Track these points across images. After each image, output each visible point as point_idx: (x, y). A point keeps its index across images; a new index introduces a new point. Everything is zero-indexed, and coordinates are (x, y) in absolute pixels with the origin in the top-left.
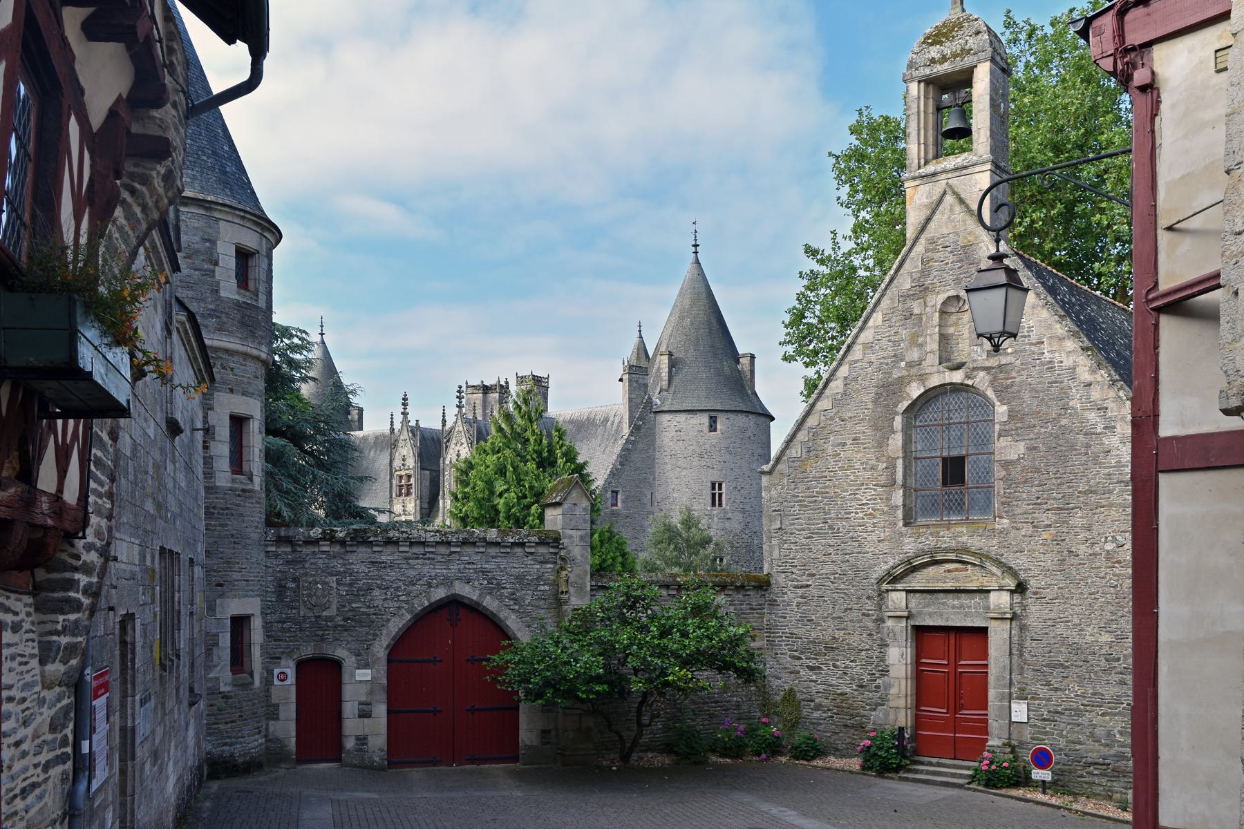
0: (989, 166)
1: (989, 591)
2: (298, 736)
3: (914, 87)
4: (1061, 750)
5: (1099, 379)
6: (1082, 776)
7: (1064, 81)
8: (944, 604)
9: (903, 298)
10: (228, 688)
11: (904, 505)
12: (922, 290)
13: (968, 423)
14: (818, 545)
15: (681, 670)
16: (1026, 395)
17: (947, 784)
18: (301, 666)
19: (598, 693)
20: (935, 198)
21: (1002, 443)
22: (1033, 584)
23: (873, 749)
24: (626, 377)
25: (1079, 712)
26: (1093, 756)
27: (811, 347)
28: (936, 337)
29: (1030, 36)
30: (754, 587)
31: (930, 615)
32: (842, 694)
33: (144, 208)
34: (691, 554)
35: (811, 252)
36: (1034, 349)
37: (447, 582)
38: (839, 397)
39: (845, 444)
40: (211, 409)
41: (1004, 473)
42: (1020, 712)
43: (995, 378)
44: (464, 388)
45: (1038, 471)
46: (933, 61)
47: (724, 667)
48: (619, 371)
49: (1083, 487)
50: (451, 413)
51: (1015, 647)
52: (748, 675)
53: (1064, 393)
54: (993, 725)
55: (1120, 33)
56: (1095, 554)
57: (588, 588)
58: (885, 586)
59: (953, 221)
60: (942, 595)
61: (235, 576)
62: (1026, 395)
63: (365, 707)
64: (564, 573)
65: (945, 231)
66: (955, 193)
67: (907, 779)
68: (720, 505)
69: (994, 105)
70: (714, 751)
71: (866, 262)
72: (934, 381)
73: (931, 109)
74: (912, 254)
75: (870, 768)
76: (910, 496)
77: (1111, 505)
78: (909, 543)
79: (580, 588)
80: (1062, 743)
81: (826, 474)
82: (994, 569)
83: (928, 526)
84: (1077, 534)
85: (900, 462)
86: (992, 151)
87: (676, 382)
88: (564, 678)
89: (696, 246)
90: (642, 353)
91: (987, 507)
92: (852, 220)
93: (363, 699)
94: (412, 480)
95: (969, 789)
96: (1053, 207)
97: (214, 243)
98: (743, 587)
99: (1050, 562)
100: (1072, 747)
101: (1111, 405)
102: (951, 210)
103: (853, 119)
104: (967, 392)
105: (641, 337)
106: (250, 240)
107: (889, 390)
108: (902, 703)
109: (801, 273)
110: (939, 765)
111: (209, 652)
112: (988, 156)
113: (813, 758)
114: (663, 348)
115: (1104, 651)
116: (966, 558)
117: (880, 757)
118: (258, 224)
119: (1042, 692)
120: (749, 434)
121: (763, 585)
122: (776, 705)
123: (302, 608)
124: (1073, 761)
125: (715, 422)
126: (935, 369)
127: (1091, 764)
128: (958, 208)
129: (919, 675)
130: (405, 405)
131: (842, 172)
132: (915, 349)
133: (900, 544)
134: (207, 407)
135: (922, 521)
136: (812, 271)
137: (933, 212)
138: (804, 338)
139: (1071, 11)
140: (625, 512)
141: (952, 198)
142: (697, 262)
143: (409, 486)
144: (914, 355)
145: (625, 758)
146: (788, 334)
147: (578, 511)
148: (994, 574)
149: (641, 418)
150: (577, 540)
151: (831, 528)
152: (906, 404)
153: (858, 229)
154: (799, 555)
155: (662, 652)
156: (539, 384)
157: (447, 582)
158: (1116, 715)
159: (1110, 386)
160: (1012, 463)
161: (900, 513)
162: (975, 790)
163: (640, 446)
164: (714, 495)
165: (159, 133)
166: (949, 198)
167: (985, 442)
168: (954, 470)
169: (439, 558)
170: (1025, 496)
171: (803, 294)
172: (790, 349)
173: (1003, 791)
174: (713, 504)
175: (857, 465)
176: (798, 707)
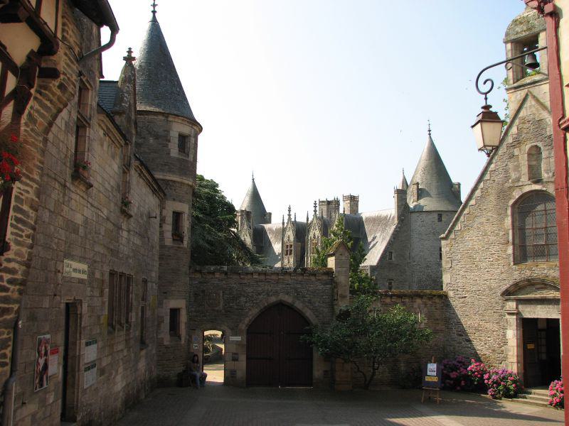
10: (168, 343)
14: (470, 276)
17: (537, 404)
20: (522, 98)
33: (51, 101)
37: (276, 293)
40: (164, 209)
61: (173, 288)
63: (236, 356)
66: (534, 97)
72: (527, 189)
89: (430, 131)
93: (235, 352)
94: (292, 248)
97: (168, 132)
106: (186, 130)
108: (515, 360)
111: (159, 325)
130: (289, 211)
134: (162, 207)
140: (396, 263)
143: (291, 251)
156: (353, 200)
157: (276, 293)
161: (511, 258)
165: (54, 66)
166: (530, 98)
169: (273, 281)
175: (489, 233)
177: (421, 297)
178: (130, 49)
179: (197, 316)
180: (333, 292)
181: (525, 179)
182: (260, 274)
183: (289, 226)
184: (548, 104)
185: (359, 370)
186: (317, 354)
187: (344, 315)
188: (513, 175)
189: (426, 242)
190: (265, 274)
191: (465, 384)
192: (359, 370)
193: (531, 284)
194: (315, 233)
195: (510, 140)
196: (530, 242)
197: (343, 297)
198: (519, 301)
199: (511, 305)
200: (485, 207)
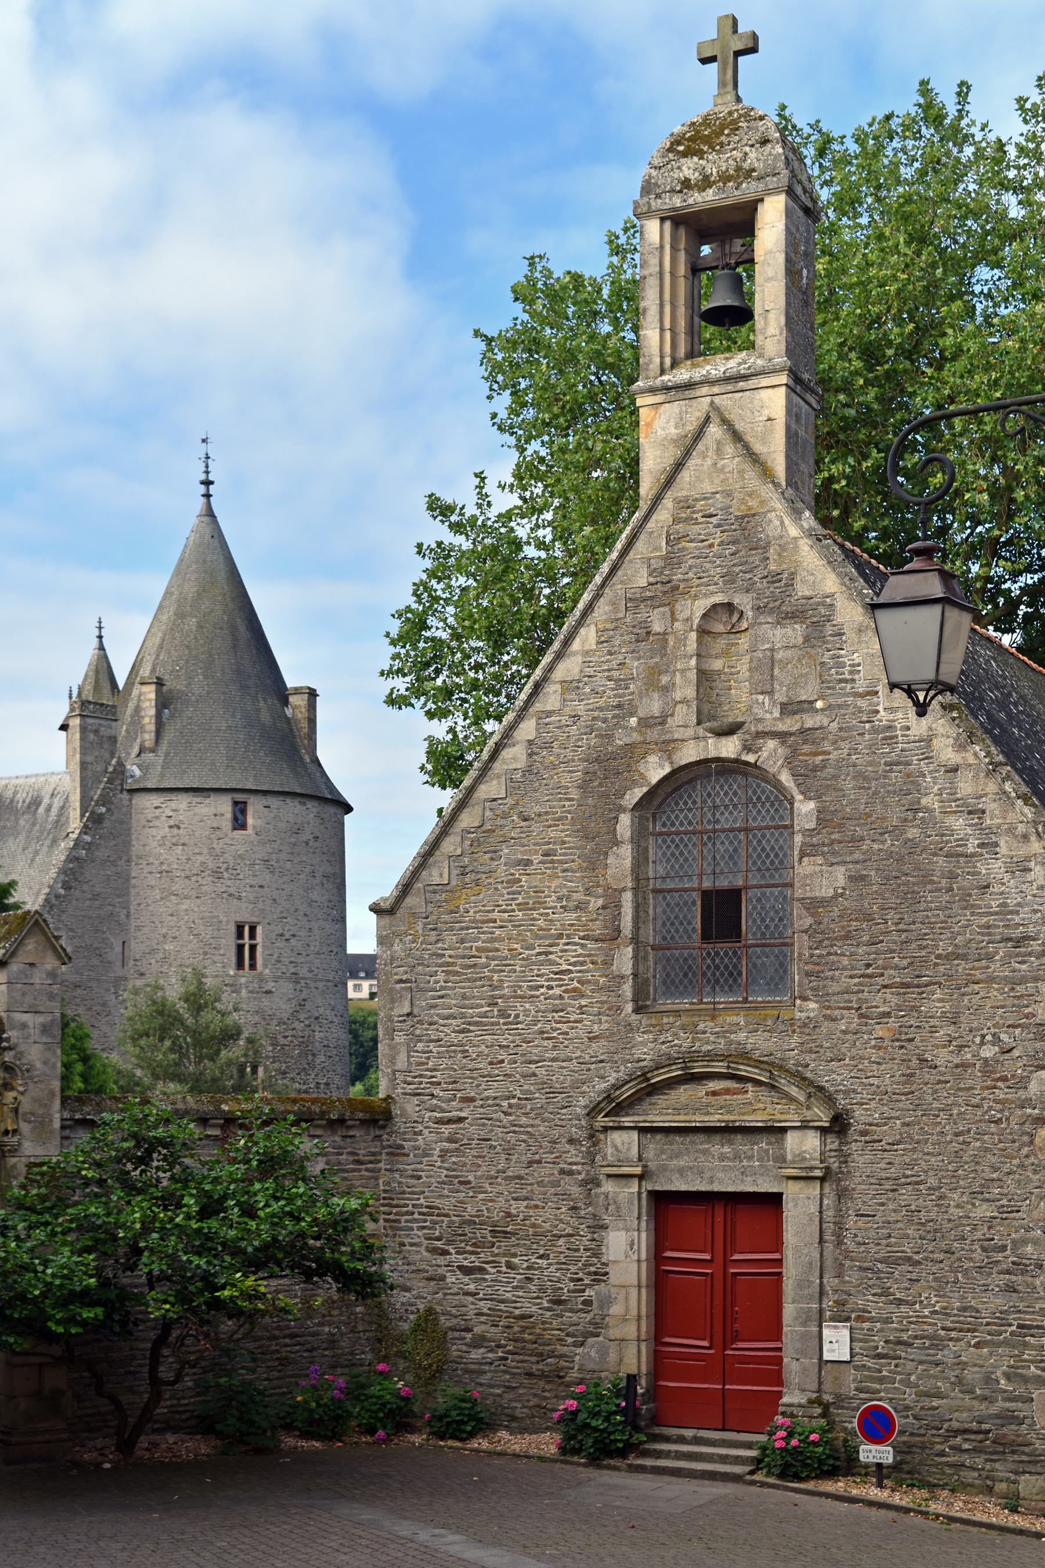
0: (783, 379)
1: (784, 1130)
3: (653, 228)
4: (907, 1408)
5: (971, 760)
6: (942, 1454)
7: (881, 237)
8: (705, 1152)
9: (635, 602)
11: (635, 975)
12: (667, 592)
13: (747, 830)
14: (479, 1044)
15: (245, 1276)
16: (848, 784)
17: (712, 1476)
19: (84, 1323)
20: (691, 427)
21: (806, 867)
22: (859, 1116)
23: (582, 1416)
24: (75, 722)
25: (937, 1343)
26: (961, 1419)
27: (439, 682)
28: (693, 675)
29: (821, 153)
30: (363, 1122)
32: (523, 1317)
34: (200, 1059)
35: (439, 508)
36: (862, 703)
38: (518, 776)
39: (528, 863)
41: (809, 921)
43: (795, 752)
45: (869, 918)
46: (686, 183)
47: (312, 1267)
48: (61, 710)
49: (943, 947)
51: (829, 1228)
52: (364, 1286)
53: (912, 784)
54: (792, 1367)
56: (964, 1065)
57: (57, 1124)
58: (601, 1121)
59: (722, 470)
60: (702, 1137)
62: (848, 785)
65: (708, 487)
66: (725, 421)
67: (642, 1469)
68: (253, 966)
69: (792, 272)
70: (289, 1427)
71: (541, 533)
72: (689, 754)
73: (682, 270)
74: (651, 525)
75: (577, 1451)
76: (645, 958)
77: (991, 980)
78: (644, 1044)
79: (41, 1125)
80: (909, 1396)
81: (495, 915)
82: (794, 1091)
83: (677, 1013)
84: (934, 1030)
86: (790, 352)
87: (169, 735)
88: (22, 1297)
89: (207, 483)
91: (779, 980)
92: (514, 456)
95: (753, 1483)
96: (866, 457)
98: (341, 1121)
99: (888, 1077)
100: (927, 1402)
101: (991, 806)
102: (719, 451)
103: (519, 273)
104: (745, 775)
105: (101, 648)
107: (609, 767)
108: (630, 1331)
109: (420, 546)
110: (697, 1441)
112: (782, 360)
113: (472, 1435)
114: (145, 671)
115: (979, 1235)
116: (745, 1070)
117: (596, 1429)
119: (876, 1306)
120: (306, 836)
121: (378, 1118)
122: (401, 1339)
124: (928, 1427)
125: (244, 812)
126: (690, 732)
127: (957, 1432)
128: (729, 449)
129: (661, 1281)
131: (496, 368)
132: (656, 695)
133: (629, 1045)
135: (668, 1003)
136: (439, 544)
137: (687, 453)
138: (422, 664)
139: (888, 118)
141: (723, 428)
142: (210, 513)
144: (654, 706)
145: (126, 1446)
146: (395, 657)
147: (38, 978)
148: (793, 1100)
149: (104, 800)
150: (35, 1034)
151: (503, 1014)
152: (638, 793)
153: (525, 474)
154: (445, 1063)
155: (205, 1244)
158: (999, 1345)
159: (989, 773)
160: (822, 902)
161: (627, 989)
162: (763, 1485)
163: (101, 854)
164: (240, 948)
166: (714, 430)
167: (775, 865)
168: (722, 913)
170: (845, 961)
171: (424, 584)
172: (401, 684)
173: (810, 1485)
174: (240, 965)
175: (551, 901)
176: (441, 1341)
178: (924, 83)
181: (684, 715)
184: (779, 466)
191: (375, 1410)
200: (537, 809)
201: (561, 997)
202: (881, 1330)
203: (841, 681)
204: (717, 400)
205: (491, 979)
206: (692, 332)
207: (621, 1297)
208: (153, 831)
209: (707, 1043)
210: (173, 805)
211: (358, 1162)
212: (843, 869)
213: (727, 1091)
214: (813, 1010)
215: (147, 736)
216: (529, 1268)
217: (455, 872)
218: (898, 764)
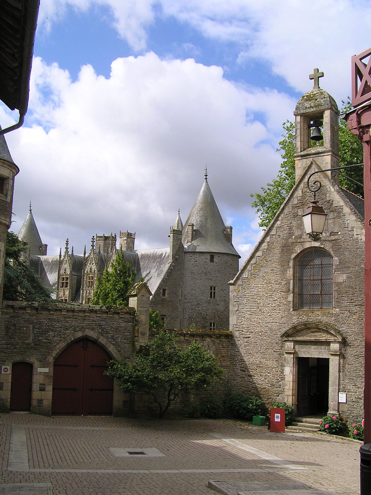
2: (11, 398)
18: (15, 365)
20: (308, 165)
31: (304, 352)
37: (82, 329)
42: (342, 398)
44: (95, 238)
50: (89, 248)
55: (359, 122)
64: (137, 327)
66: (316, 164)
68: (214, 297)
72: (307, 245)
81: (259, 285)
85: (292, 281)
89: (206, 176)
90: (180, 223)
91: (330, 303)
93: (42, 382)
94: (69, 281)
108: (290, 393)
118: (10, 166)
123: (16, 338)
125: (213, 258)
130: (67, 244)
143: (67, 283)
154: (246, 323)
157: (82, 329)
160: (340, 283)
166: (314, 166)
174: (211, 297)
177: (210, 336)
179: (7, 349)
180: (134, 329)
182: (68, 311)
183: (66, 259)
185: (155, 400)
186: (117, 386)
187: (144, 351)
188: (297, 233)
189: (198, 281)
190: (73, 311)
192: (155, 400)
193: (307, 327)
194: (92, 267)
195: (295, 201)
196: (308, 290)
197: (143, 334)
198: (296, 342)
199: (289, 345)
200: (270, 259)
201: (275, 307)
202: (354, 395)
203: (345, 227)
204: (314, 158)
205: (258, 301)
206: (308, 142)
207: (288, 384)
208: (190, 263)
209: (311, 319)
210: (195, 256)
211: (224, 347)
212: (345, 275)
213: (316, 332)
214: (337, 311)
215: (189, 238)
216: (265, 376)
217: (249, 274)
218: (359, 248)
